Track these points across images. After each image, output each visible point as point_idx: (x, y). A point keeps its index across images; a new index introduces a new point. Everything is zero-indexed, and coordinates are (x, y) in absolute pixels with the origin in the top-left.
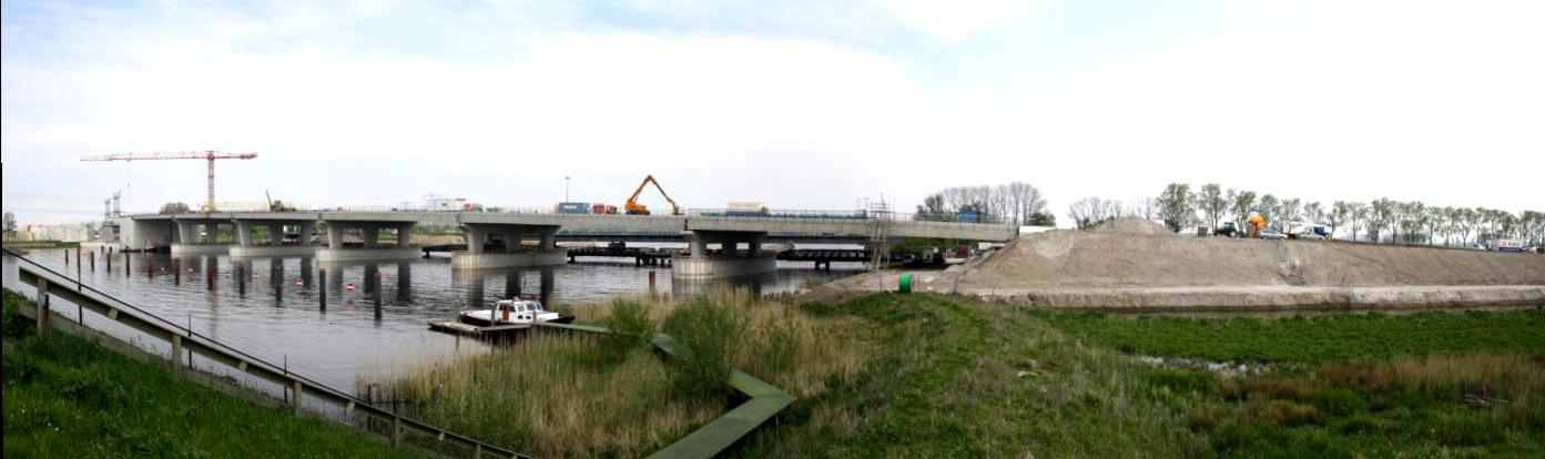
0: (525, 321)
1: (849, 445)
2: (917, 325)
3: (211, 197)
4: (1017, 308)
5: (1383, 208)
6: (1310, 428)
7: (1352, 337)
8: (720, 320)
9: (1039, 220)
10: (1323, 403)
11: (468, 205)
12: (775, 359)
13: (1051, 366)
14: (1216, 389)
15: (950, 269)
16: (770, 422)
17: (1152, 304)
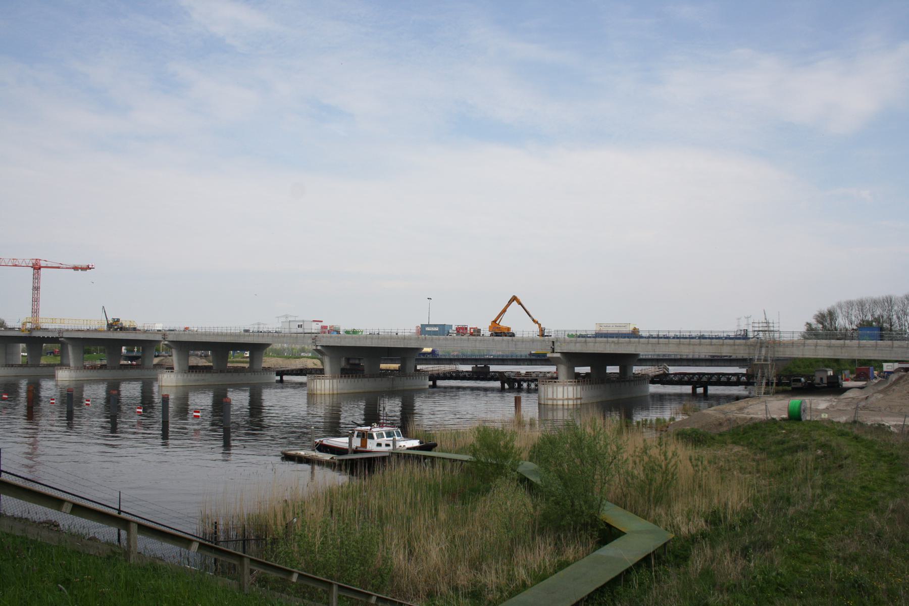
0: (384, 448)
2: (810, 457)
3: (35, 311)
8: (589, 448)
11: (325, 327)
12: (650, 492)
15: (848, 394)
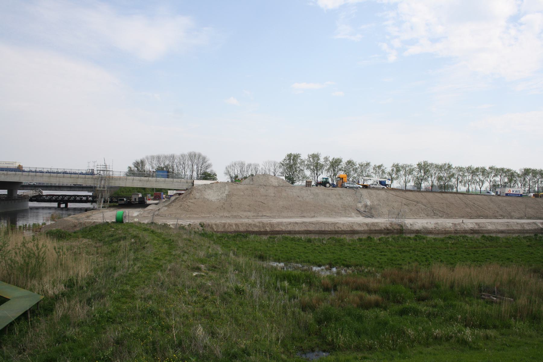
1: (81, 326)
2: (128, 244)
4: (193, 232)
5: (424, 168)
6: (377, 310)
7: (404, 252)
9: (206, 176)
10: (386, 294)
13: (213, 268)
14: (317, 283)
15: (149, 208)
16: (25, 315)
17: (277, 229)
